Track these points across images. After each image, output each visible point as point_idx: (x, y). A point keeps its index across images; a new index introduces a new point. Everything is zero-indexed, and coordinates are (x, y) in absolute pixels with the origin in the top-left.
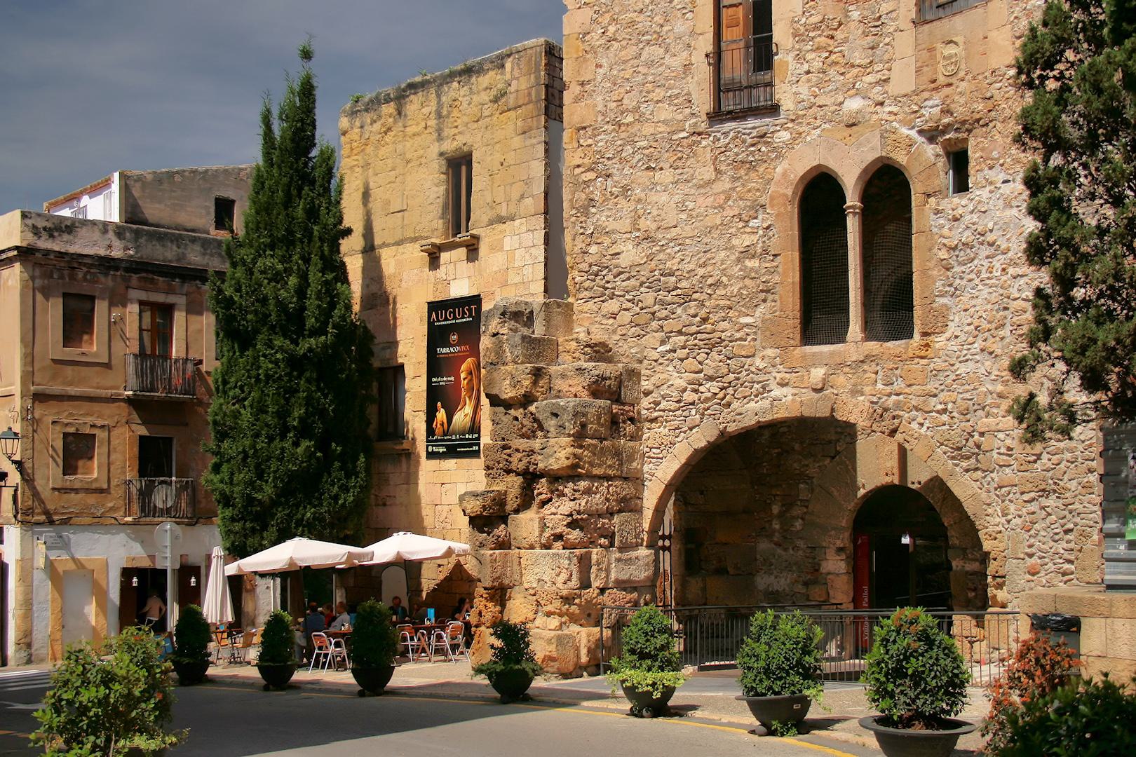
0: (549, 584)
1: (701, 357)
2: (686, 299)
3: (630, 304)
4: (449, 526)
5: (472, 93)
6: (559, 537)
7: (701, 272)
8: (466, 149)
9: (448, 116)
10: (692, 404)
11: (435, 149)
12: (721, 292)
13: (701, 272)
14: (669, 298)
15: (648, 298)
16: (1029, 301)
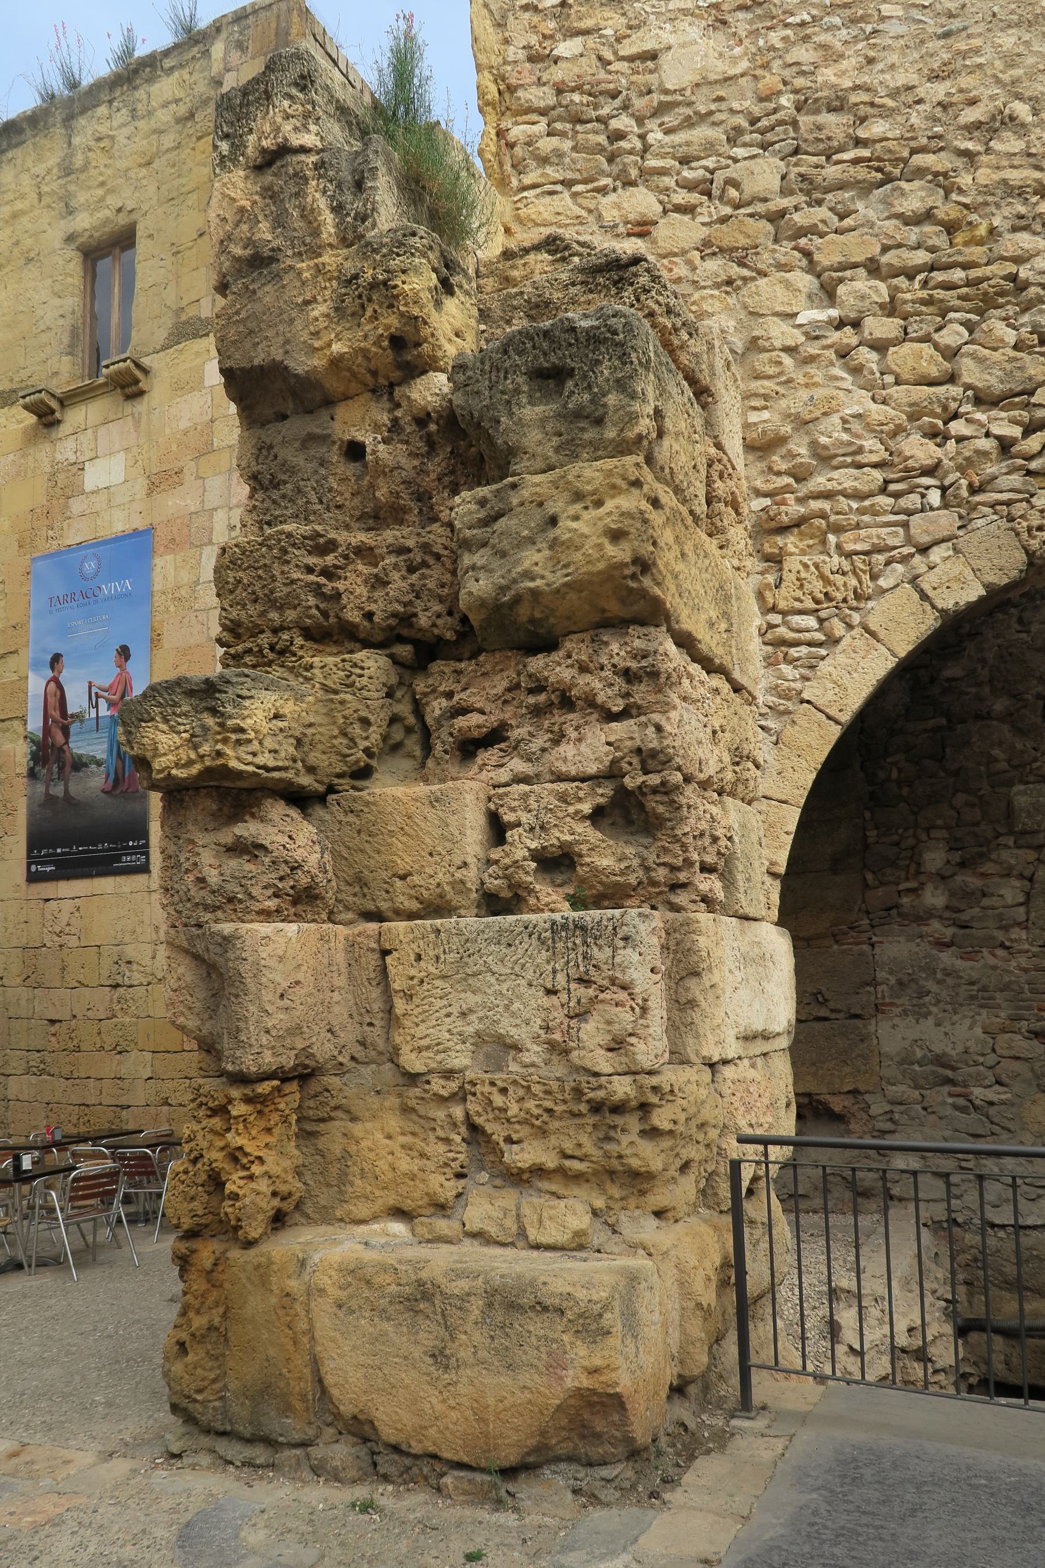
0: (534, 1053)
1: (953, 335)
2: (886, 172)
3: (694, 198)
4: (73, 942)
5: (134, 113)
6: (556, 862)
7: (940, 90)
8: (122, 220)
9: (85, 168)
10: (929, 471)
11: (54, 236)
12: (1009, 143)
13: (940, 90)
14: (832, 172)
15: (764, 174)
16: (894, 655)
